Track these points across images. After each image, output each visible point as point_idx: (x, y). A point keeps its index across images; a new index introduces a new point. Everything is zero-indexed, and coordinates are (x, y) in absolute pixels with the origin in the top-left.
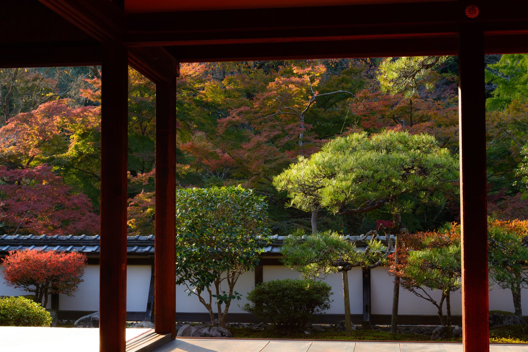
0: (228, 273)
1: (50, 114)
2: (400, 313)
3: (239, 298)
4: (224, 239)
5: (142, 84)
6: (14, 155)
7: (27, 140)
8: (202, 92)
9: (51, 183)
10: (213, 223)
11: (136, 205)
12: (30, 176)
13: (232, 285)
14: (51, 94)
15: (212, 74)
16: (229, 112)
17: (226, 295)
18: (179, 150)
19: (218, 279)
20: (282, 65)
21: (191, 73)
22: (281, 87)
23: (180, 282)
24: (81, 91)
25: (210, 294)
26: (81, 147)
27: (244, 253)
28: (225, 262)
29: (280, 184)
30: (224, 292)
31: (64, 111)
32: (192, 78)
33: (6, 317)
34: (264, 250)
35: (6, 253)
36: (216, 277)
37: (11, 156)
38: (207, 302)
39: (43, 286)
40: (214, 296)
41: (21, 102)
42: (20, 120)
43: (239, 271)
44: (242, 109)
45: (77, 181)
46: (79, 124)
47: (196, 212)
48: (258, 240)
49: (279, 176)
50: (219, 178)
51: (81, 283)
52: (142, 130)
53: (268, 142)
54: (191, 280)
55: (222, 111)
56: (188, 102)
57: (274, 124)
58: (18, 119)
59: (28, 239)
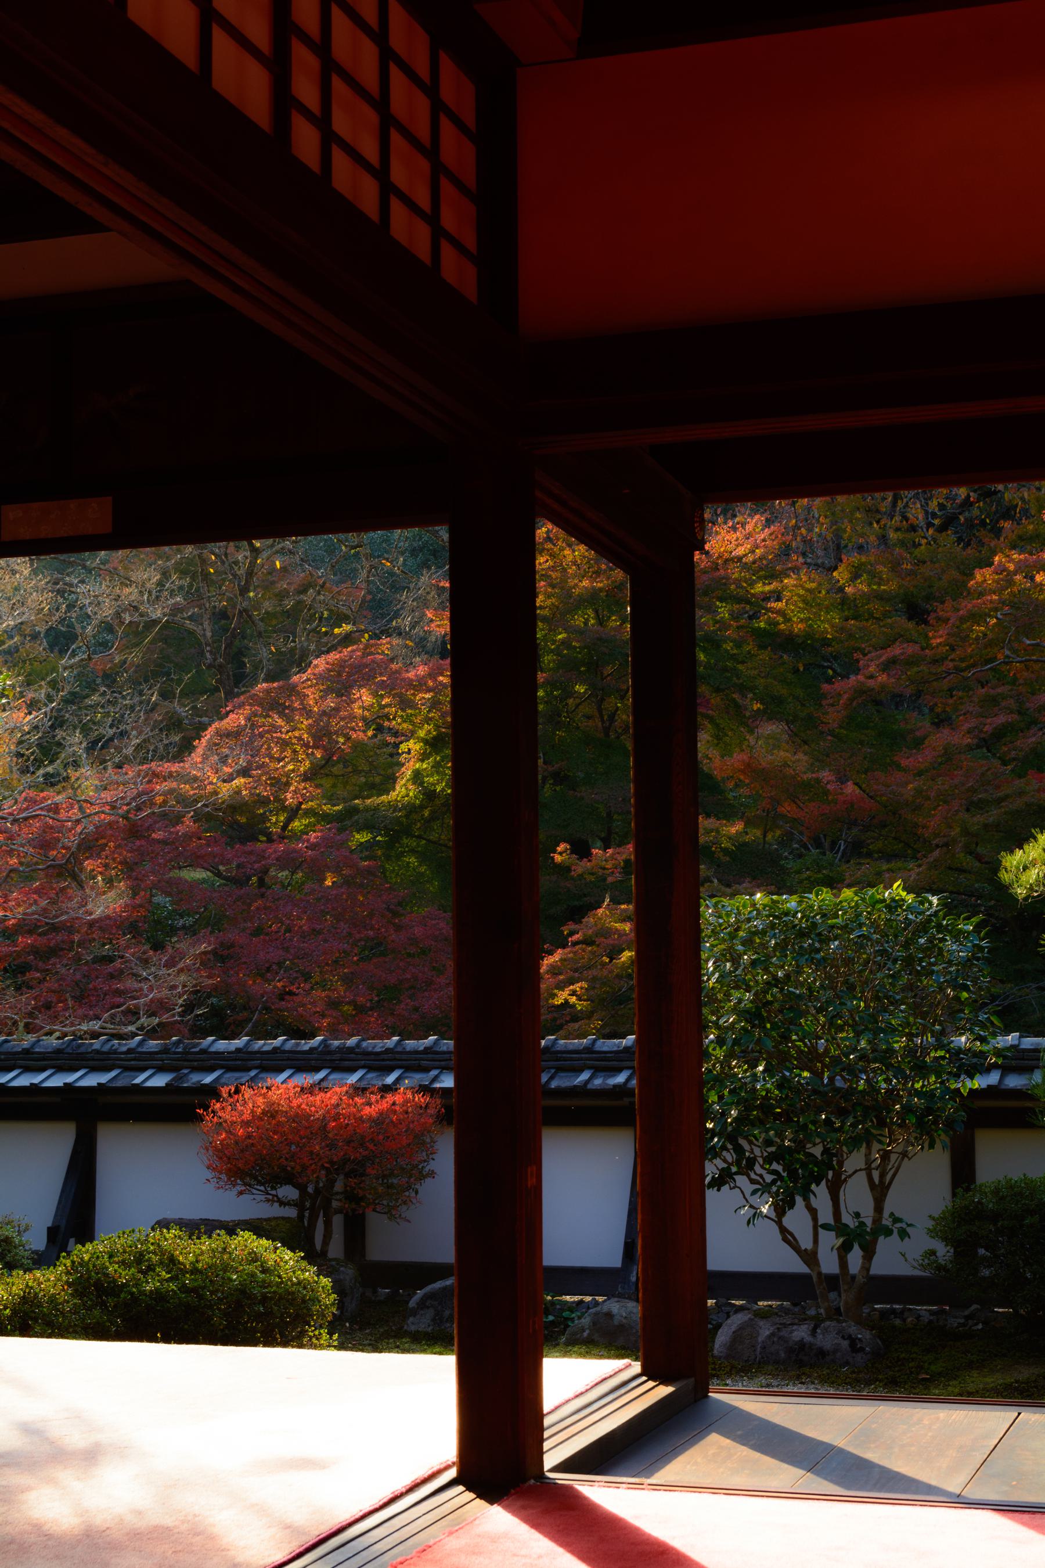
0: (868, 1155)
1: (341, 683)
3: (903, 1234)
4: (854, 1050)
5: (601, 590)
6: (246, 804)
7: (280, 760)
8: (773, 605)
9: (347, 882)
10: (817, 999)
11: (587, 942)
12: (290, 861)
13: (880, 1191)
14: (347, 628)
15: (804, 554)
16: (857, 661)
17: (862, 1224)
18: (709, 777)
19: (838, 1174)
20: (1012, 518)
21: (740, 551)
22: (1010, 582)
23: (718, 1183)
24: (429, 614)
25: (815, 1219)
26: (432, 776)
27: (918, 1093)
28: (858, 1122)
29: (1024, 878)
30: (857, 1215)
31: (381, 675)
32: (746, 567)
33: (201, 1297)
34: (977, 1083)
35: (212, 1092)
36: (832, 1168)
37: (235, 806)
38: (806, 1244)
39: (317, 1190)
40: (826, 1227)
41: (265, 652)
42: (261, 705)
43: (900, 1149)
44: (896, 650)
45: (422, 874)
46: (425, 710)
47: (766, 970)
48: (959, 1051)
49: (1019, 853)
50: (829, 855)
51: (428, 1180)
52: (603, 721)
53: (978, 747)
54: (753, 1176)
55: (835, 658)
56: (735, 636)
57: (992, 692)
58: (256, 700)
59: (275, 1050)
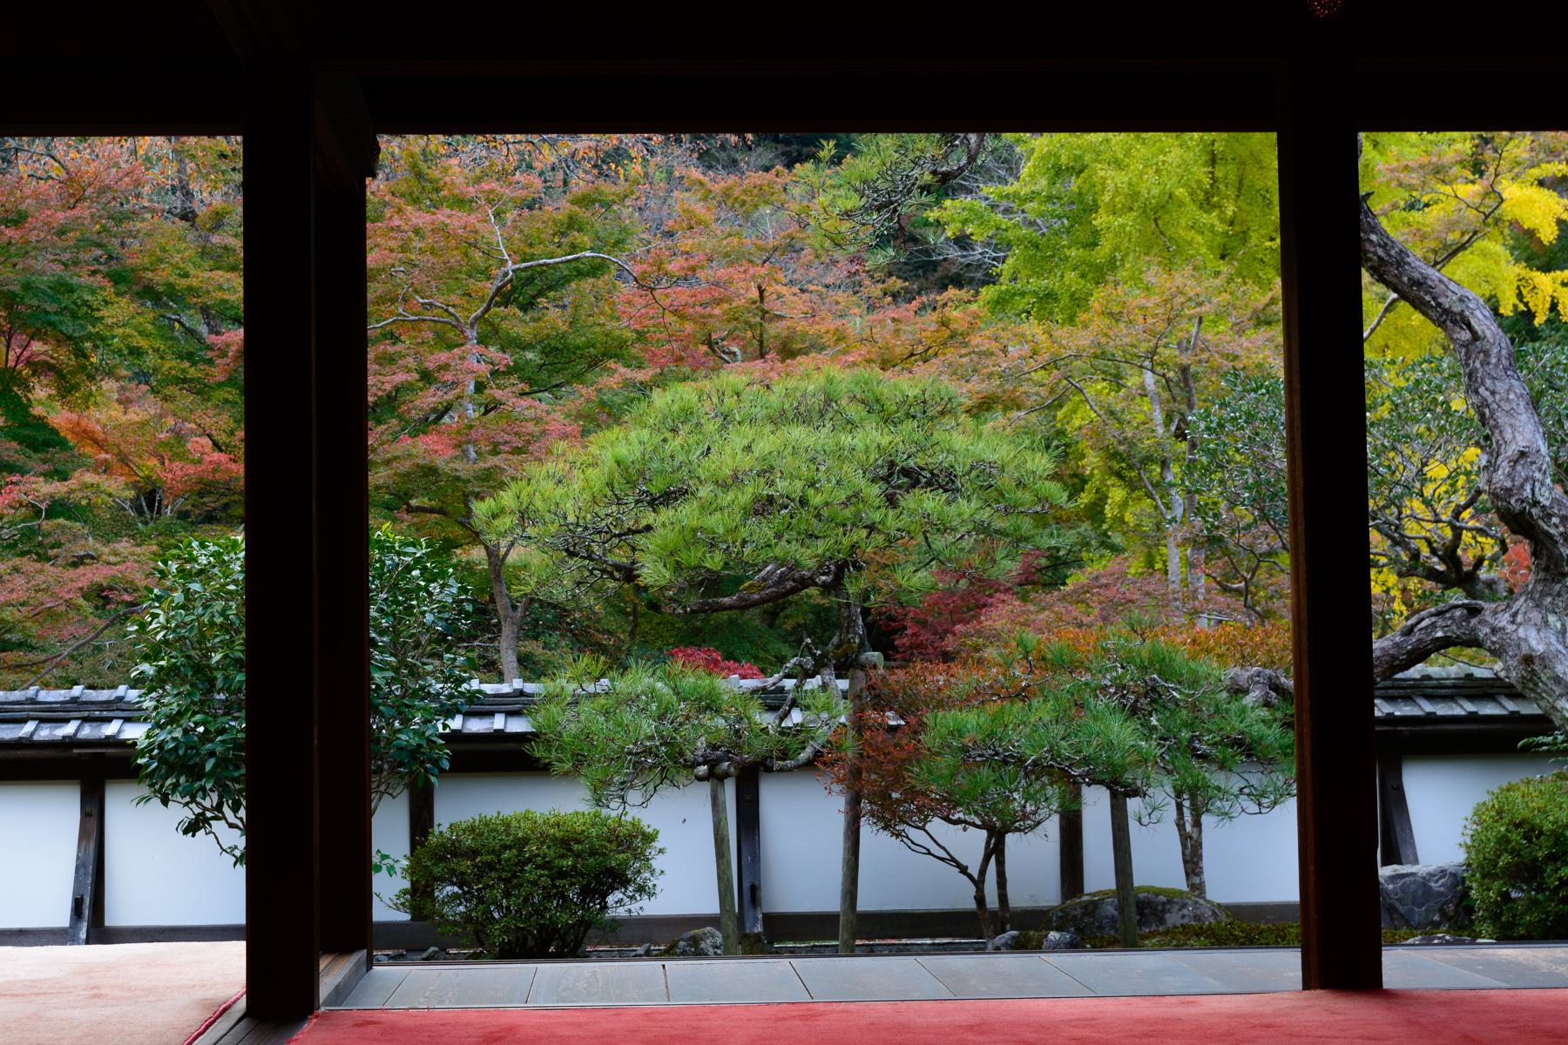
2: (865, 904)
